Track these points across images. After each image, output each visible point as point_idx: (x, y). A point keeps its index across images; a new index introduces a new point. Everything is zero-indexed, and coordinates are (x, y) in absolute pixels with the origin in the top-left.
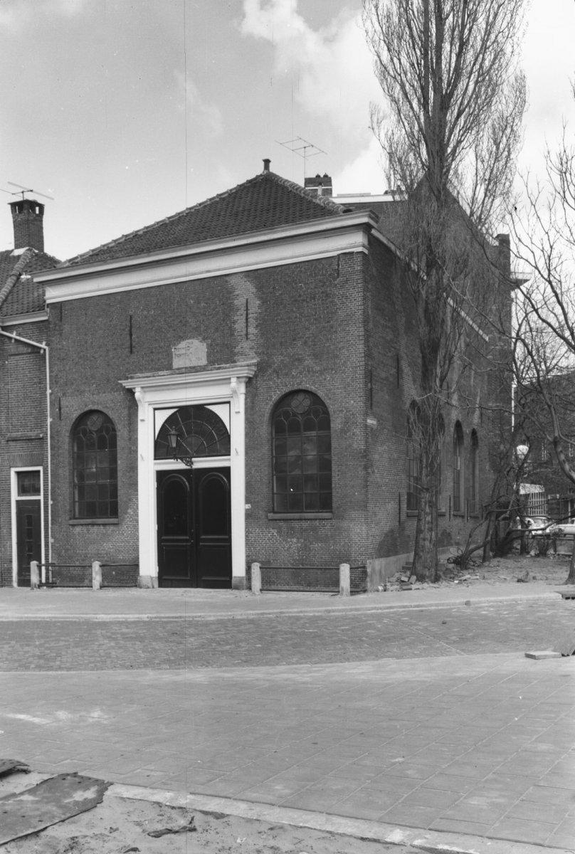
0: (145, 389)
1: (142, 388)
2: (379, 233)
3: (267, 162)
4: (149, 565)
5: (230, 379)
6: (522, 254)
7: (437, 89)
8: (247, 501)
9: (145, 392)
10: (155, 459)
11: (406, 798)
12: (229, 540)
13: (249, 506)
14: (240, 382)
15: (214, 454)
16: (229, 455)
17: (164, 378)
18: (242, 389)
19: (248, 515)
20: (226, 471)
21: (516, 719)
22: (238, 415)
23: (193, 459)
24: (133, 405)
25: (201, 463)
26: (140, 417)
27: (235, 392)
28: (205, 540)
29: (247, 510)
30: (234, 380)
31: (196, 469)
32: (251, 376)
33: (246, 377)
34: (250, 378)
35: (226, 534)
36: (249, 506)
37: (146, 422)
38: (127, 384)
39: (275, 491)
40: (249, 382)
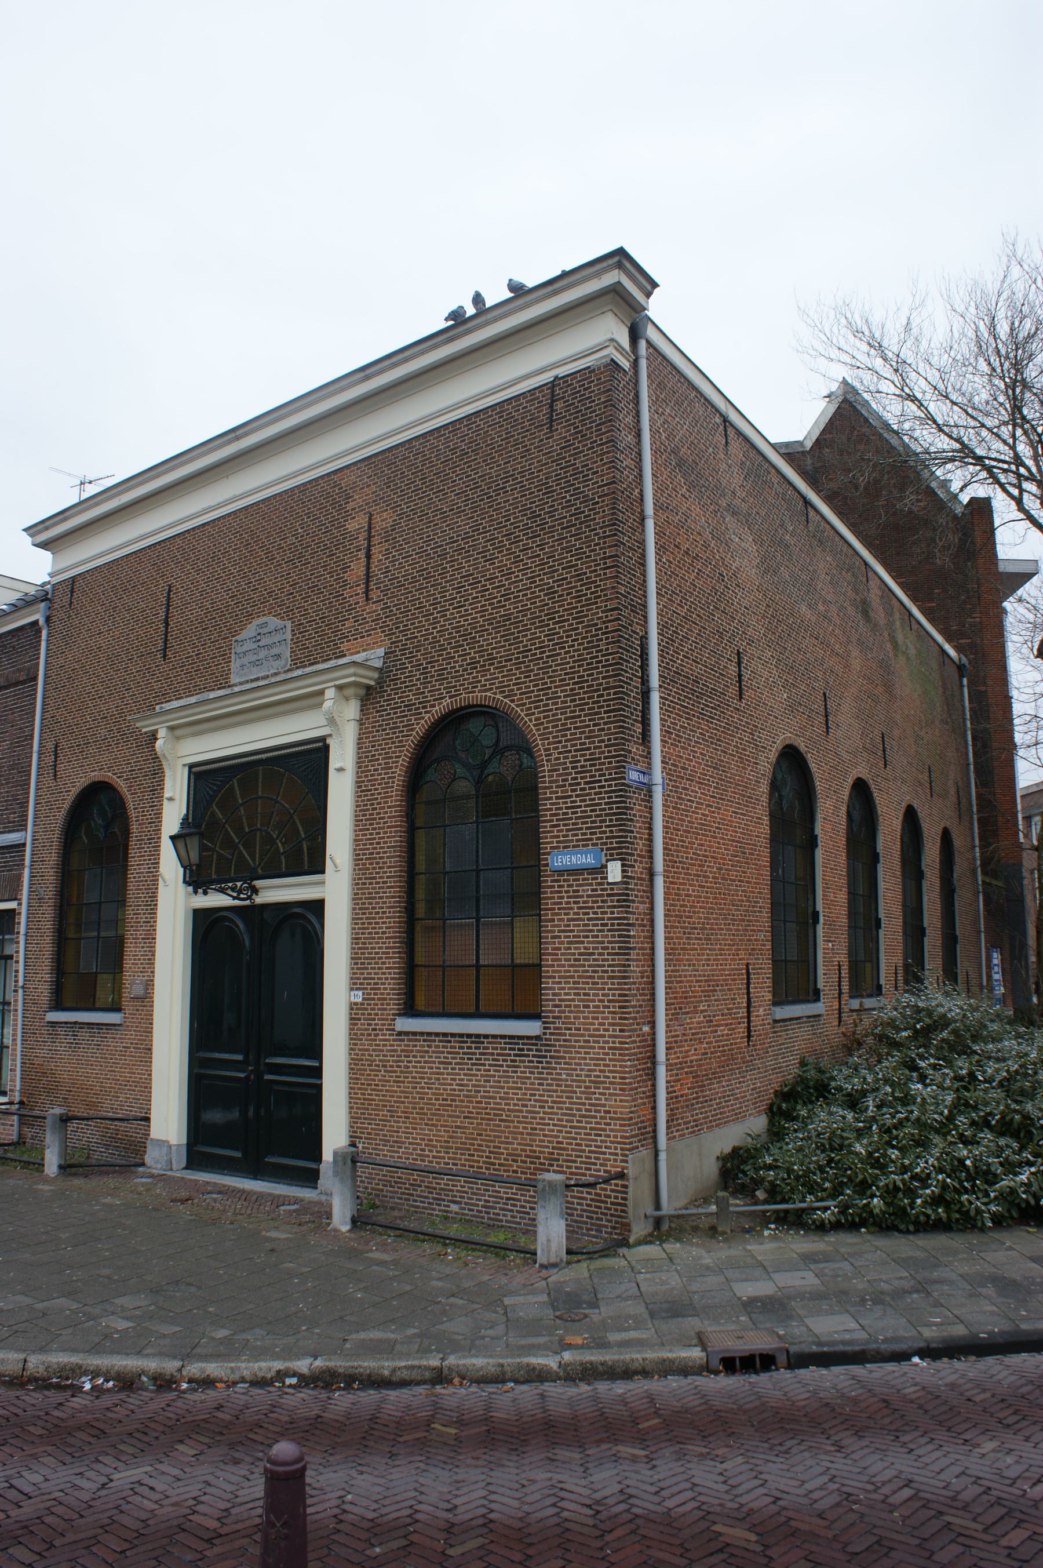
0: (178, 732)
1: (171, 729)
2: (1035, 933)
4: (168, 1120)
5: (321, 693)
6: (1017, 1530)
9: (178, 738)
13: (358, 997)
14: (347, 699)
16: (323, 872)
17: (215, 701)
18: (352, 710)
19: (355, 1013)
20: (317, 907)
21: (1035, 1000)
22: (341, 774)
23: (258, 883)
25: (276, 892)
26: (167, 794)
27: (332, 721)
29: (353, 1006)
30: (330, 693)
31: (265, 907)
32: (372, 683)
34: (368, 688)
36: (358, 997)
37: (177, 802)
38: (146, 726)
40: (369, 696)
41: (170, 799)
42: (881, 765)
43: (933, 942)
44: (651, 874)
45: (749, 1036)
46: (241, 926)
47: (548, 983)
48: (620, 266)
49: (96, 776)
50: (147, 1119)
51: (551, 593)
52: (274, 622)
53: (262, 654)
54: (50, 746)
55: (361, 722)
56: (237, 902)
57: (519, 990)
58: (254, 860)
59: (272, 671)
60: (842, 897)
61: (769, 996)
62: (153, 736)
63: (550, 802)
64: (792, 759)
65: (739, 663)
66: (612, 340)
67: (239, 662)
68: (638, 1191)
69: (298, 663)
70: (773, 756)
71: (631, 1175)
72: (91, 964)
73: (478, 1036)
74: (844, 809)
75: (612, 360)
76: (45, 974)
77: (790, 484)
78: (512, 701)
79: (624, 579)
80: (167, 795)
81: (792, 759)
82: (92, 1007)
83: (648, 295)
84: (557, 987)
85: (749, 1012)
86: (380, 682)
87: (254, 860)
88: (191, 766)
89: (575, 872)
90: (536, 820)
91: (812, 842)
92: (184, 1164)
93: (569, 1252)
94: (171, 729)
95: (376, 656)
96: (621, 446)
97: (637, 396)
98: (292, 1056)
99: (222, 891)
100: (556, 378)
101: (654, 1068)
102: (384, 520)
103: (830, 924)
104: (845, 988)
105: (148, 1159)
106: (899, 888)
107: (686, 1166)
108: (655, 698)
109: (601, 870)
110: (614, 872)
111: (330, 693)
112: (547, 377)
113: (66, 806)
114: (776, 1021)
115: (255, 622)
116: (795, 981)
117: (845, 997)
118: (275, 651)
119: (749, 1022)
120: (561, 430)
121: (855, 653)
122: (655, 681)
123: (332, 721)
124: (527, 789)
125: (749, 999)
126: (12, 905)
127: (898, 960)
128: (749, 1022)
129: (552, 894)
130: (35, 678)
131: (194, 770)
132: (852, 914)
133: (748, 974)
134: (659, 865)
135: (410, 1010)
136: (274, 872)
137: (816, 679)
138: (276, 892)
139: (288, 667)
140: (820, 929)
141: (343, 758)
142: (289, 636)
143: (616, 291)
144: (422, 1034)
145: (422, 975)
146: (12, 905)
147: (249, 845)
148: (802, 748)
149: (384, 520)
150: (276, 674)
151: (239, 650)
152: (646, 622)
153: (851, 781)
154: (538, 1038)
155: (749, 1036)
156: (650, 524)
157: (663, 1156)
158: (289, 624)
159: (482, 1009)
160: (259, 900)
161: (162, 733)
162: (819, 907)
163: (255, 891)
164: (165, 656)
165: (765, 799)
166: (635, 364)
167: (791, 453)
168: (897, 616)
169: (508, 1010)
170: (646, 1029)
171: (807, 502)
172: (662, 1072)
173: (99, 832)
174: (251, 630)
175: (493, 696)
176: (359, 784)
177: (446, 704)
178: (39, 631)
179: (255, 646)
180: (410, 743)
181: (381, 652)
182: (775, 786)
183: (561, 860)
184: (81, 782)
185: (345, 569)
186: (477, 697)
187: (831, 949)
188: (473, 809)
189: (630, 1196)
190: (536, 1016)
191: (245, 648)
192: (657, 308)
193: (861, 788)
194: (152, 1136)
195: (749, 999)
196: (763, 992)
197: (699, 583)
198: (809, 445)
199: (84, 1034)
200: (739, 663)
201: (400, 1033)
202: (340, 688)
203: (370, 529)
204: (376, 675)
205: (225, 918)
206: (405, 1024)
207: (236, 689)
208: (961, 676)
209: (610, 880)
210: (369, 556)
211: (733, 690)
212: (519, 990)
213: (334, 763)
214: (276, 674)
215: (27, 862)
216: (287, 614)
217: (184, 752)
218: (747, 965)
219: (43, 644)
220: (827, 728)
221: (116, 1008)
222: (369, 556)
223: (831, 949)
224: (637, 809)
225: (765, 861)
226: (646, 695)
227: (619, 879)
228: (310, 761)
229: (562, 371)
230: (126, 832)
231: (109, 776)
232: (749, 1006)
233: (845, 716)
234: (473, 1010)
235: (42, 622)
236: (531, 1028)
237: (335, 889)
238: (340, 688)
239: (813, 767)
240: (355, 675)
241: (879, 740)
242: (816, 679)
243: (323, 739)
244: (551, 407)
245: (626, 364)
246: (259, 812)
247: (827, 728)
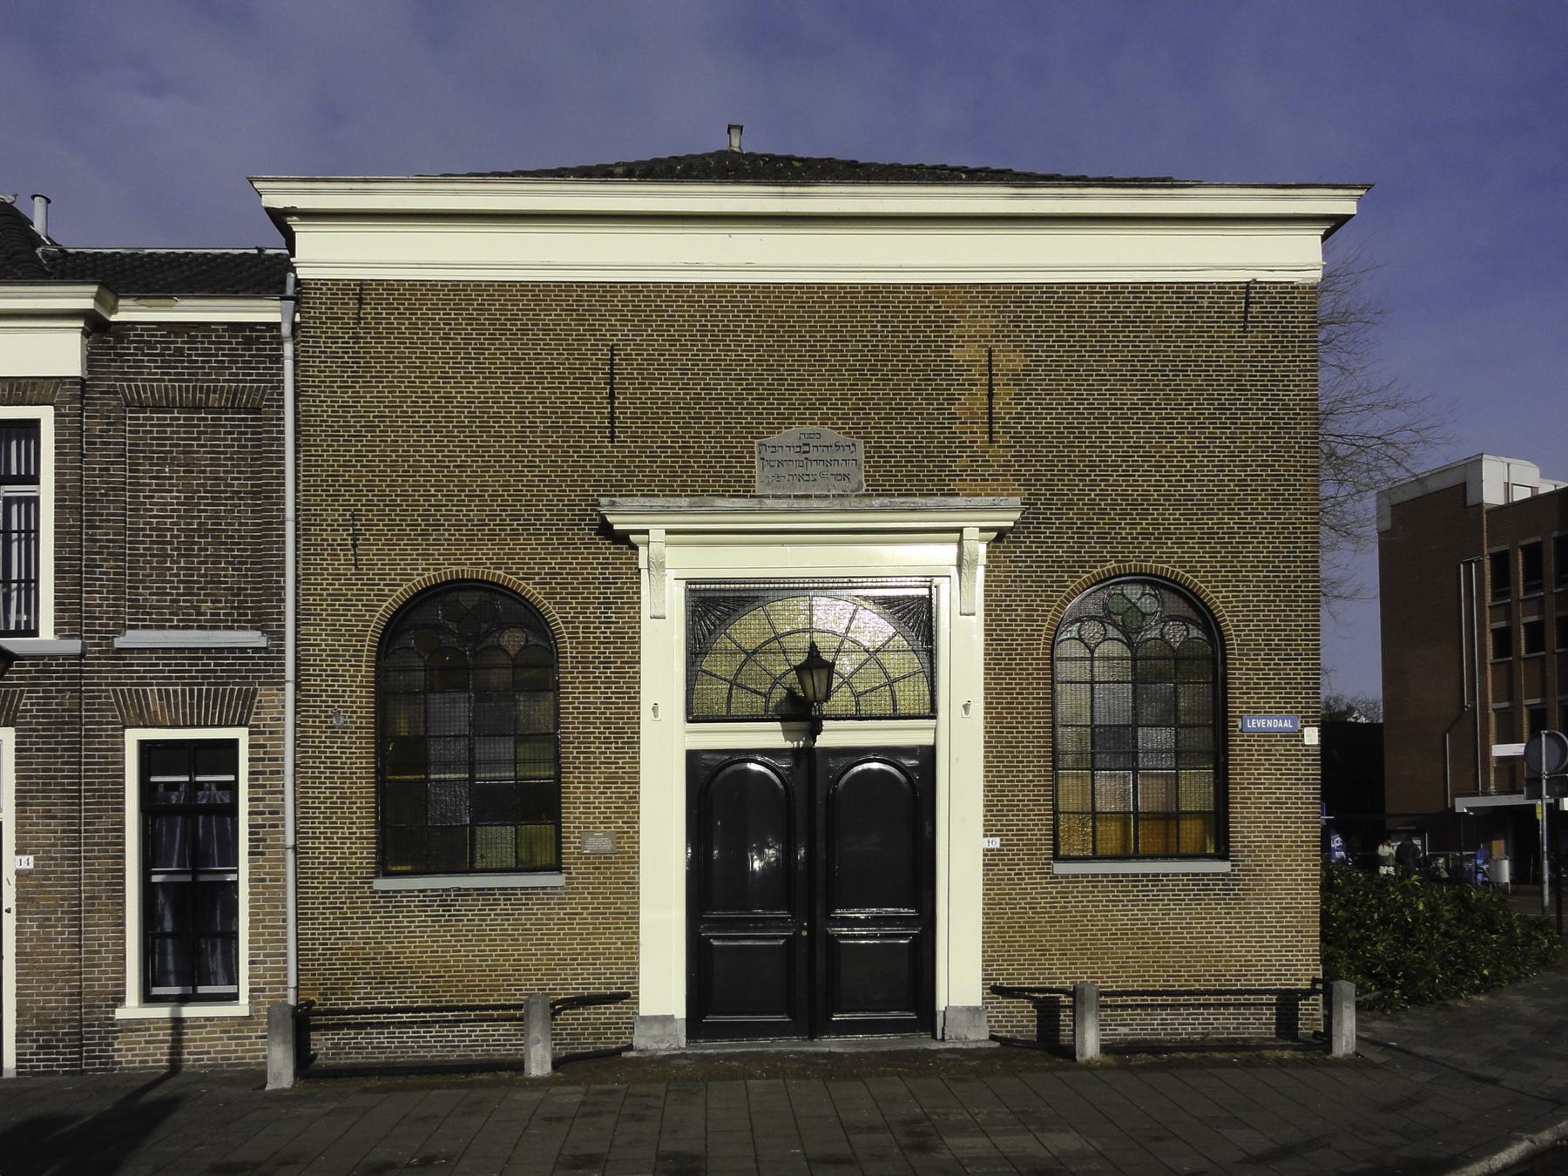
4: (663, 987)
8: (988, 832)
13: (996, 843)
16: (693, 757)
17: (728, 513)
29: (987, 852)
51: (1242, 484)
59: (833, 492)
63: (1238, 674)
82: (471, 870)
88: (690, 582)
102: (1010, 360)
109: (1298, 735)
118: (835, 469)
120: (1255, 334)
139: (863, 491)
149: (1010, 360)
159: (1099, 852)
160: (823, 741)
164: (612, 437)
174: (791, 435)
178: (280, 341)
179: (797, 457)
185: (951, 399)
191: (779, 456)
210: (991, 395)
221: (557, 868)
222: (991, 395)
229: (1264, 277)
234: (511, 862)
235: (286, 330)
236: (1224, 867)
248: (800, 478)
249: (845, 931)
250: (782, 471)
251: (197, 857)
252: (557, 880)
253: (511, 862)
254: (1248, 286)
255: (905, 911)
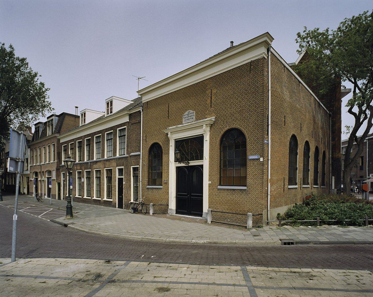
0: (172, 133)
1: (171, 132)
3: (232, 42)
4: (173, 205)
5: (203, 125)
7: (324, 230)
9: (172, 134)
10: (203, 165)
11: (340, 146)
12: (202, 196)
14: (207, 127)
15: (292, 184)
16: (203, 160)
18: (208, 129)
20: (202, 166)
24: (168, 140)
25: (193, 163)
27: (205, 131)
28: (193, 196)
30: (204, 126)
33: (209, 124)
34: (212, 125)
35: (201, 194)
39: (222, 176)
40: (211, 126)
41: (171, 146)
42: (311, 138)
43: (320, 174)
44: (268, 160)
45: (284, 191)
46: (186, 170)
47: (248, 180)
48: (267, 36)
49: (155, 141)
50: (168, 205)
51: (249, 106)
52: (191, 111)
53: (189, 118)
54: (145, 135)
55: (210, 131)
56: (186, 165)
57: (242, 181)
58: (188, 157)
60: (302, 165)
61: (288, 184)
62: (167, 134)
63: (248, 146)
64: (294, 137)
65: (285, 118)
66: (264, 53)
67: (184, 119)
68: (264, 217)
69: (197, 119)
70: (290, 137)
71: (263, 214)
72: (156, 176)
73: (234, 189)
74: (303, 147)
75: (264, 57)
76: (146, 179)
77: (296, 78)
78: (241, 127)
79: (265, 103)
80: (170, 145)
81: (294, 137)
83: (272, 41)
84: (249, 181)
85: (284, 186)
86: (214, 123)
87: (188, 157)
88: (175, 140)
89: (254, 160)
90: (246, 150)
91: (297, 154)
92: (175, 213)
93: (253, 227)
94: (171, 132)
95: (213, 118)
96: (265, 75)
97: (268, 64)
98: (196, 193)
99: (183, 163)
100: (252, 61)
101: (268, 196)
103: (299, 170)
104: (302, 183)
105: (168, 212)
106: (313, 163)
107: (273, 213)
108: (270, 126)
109: (259, 159)
110: (261, 159)
111: (204, 126)
112: (249, 61)
113: (149, 147)
114: (289, 188)
115: (187, 111)
116: (292, 181)
117: (302, 184)
118: (192, 117)
119: (284, 188)
121: (307, 114)
122: (270, 123)
123: (205, 131)
124: (244, 144)
125: (284, 184)
126: (138, 166)
127: (313, 178)
128: (284, 188)
129: (248, 163)
130: (140, 122)
131: (176, 140)
132: (304, 168)
133: (284, 179)
134: (270, 158)
135: (220, 185)
136: (193, 159)
137: (299, 121)
138: (193, 163)
140: (297, 171)
141: (207, 138)
142: (195, 114)
143: (266, 42)
144: (223, 189)
145: (222, 178)
146: (138, 166)
147: (188, 155)
148: (296, 135)
150: (192, 122)
151: (184, 117)
152: (268, 111)
153: (305, 141)
154: (246, 190)
155: (284, 191)
156: (270, 92)
157: (269, 211)
158: (195, 112)
160: (190, 165)
161: (169, 133)
162: (298, 166)
163: (189, 163)
165: (288, 145)
166: (268, 57)
167: (293, 67)
168: (317, 105)
169: (240, 185)
170: (266, 188)
171: (300, 82)
172: (269, 196)
173: (156, 153)
174: (187, 113)
175: (238, 126)
176: (210, 143)
177: (228, 128)
178: (141, 112)
179: (188, 116)
180: (221, 135)
181: (214, 117)
182: (290, 143)
183: (251, 157)
184: (152, 143)
185: (206, 101)
186: (234, 126)
187: (299, 175)
188: (234, 147)
189: (263, 218)
190: (246, 186)
192: (273, 44)
193: (307, 143)
194: (169, 208)
195: (284, 184)
196: (287, 183)
197: (278, 103)
198: (297, 63)
199: (154, 190)
200: (285, 118)
201: (219, 189)
202: (206, 125)
203: (211, 92)
204: (213, 122)
205: (197, 168)
206: (219, 187)
207: (184, 125)
208: (330, 117)
209: (261, 161)
210: (211, 98)
211: (283, 124)
212: (242, 181)
213: (205, 139)
214: (192, 122)
215: (141, 158)
216: (194, 110)
217: (173, 137)
218: (284, 177)
219: (142, 115)
220: (301, 130)
222: (211, 98)
223: (299, 175)
224: (266, 148)
225: (288, 158)
226: (268, 126)
227: (262, 161)
228: (200, 139)
229: (253, 59)
230: (162, 152)
231: (157, 141)
232: (284, 185)
233: (305, 128)
237: (206, 163)
238: (206, 125)
239: (298, 139)
240: (210, 122)
241: (311, 132)
242: (299, 121)
243: (202, 134)
244: (250, 67)
245: (266, 57)
246: (190, 148)
247: (301, 130)
248: (187, 120)
249: (39, 154)
250: (186, 119)
251: (86, 136)
252: (161, 187)
253: (159, 185)
254: (251, 62)
255: (2, 153)
